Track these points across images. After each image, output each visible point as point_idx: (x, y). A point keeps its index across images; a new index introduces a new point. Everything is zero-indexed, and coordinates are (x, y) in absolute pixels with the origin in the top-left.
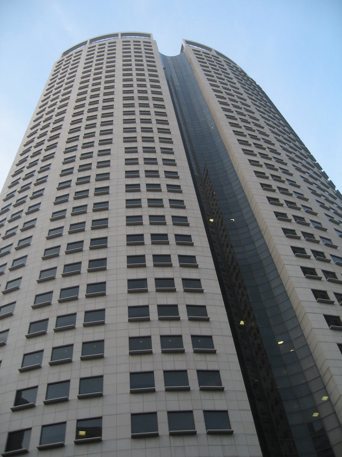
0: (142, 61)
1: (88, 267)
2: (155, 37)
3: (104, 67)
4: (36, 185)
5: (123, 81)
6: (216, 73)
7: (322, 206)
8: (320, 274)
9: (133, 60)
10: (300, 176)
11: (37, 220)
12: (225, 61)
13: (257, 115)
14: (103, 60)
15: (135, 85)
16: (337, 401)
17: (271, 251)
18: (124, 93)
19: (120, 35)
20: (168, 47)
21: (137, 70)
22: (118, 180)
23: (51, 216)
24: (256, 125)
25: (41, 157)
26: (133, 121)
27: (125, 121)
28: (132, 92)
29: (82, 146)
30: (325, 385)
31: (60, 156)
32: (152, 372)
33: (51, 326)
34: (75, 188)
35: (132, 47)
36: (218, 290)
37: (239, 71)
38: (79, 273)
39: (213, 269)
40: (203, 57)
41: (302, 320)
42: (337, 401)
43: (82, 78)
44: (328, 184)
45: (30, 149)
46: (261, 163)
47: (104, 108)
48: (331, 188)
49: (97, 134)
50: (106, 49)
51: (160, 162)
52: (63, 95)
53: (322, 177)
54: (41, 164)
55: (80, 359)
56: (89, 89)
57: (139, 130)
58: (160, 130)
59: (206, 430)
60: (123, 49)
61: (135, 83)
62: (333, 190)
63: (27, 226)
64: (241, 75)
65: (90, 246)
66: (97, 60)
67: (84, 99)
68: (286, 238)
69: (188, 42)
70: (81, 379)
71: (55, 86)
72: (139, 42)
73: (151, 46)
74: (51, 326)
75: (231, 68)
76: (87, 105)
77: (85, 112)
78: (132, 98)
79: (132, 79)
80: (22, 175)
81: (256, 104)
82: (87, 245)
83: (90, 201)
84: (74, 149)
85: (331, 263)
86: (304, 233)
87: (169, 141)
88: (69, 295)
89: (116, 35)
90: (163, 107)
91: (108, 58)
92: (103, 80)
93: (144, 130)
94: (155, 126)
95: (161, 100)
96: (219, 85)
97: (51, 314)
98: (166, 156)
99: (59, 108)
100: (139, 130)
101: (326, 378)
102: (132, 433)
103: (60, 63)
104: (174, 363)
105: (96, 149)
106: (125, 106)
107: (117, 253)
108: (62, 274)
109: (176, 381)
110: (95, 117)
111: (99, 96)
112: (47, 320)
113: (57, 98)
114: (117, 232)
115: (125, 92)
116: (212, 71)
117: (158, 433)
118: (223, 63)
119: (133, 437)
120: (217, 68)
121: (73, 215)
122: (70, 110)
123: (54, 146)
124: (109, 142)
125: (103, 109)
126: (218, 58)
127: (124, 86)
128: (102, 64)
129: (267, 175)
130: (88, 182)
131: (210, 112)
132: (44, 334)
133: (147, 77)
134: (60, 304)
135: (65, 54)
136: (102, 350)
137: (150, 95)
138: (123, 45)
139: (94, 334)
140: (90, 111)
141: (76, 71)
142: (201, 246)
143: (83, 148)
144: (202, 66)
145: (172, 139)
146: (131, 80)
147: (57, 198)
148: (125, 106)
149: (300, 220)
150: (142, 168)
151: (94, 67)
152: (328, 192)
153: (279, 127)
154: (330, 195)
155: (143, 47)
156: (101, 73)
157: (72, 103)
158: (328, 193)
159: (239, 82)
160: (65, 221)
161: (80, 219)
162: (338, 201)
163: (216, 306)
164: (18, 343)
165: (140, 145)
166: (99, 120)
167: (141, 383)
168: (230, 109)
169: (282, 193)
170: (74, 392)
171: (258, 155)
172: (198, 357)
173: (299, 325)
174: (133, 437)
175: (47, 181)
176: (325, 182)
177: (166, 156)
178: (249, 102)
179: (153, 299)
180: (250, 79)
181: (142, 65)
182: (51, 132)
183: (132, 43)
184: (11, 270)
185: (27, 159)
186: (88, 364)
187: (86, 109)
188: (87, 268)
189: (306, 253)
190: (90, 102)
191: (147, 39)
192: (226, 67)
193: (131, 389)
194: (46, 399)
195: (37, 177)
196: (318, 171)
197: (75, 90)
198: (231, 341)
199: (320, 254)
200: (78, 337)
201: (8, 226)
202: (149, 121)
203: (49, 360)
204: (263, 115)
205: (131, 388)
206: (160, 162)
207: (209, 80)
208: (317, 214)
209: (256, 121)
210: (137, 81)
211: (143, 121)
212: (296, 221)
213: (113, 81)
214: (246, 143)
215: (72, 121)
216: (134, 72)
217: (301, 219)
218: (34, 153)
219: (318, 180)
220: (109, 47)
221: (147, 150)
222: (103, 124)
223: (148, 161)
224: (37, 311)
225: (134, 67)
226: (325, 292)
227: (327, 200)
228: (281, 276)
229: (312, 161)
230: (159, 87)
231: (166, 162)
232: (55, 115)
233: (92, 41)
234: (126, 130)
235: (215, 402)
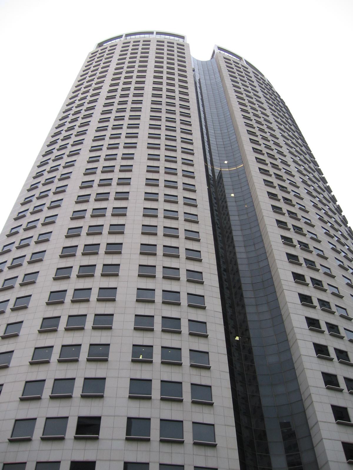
1: (105, 249)
2: (188, 40)
3: (136, 67)
4: (76, 136)
5: (155, 72)
6: (236, 66)
7: (321, 219)
8: (302, 261)
9: (165, 63)
10: (322, 227)
11: (46, 253)
12: (254, 72)
13: (274, 126)
14: (138, 49)
15: (164, 90)
16: (314, 426)
17: (273, 274)
18: (154, 78)
19: (155, 33)
20: (200, 52)
21: (168, 54)
22: (138, 188)
23: (81, 184)
24: (272, 135)
25: (74, 132)
26: (160, 103)
27: (154, 95)
28: (162, 72)
30: (305, 409)
31: (85, 154)
32: (149, 419)
33: (63, 324)
34: (96, 190)
35: (166, 48)
36: (219, 308)
37: (265, 84)
38: (97, 253)
39: (217, 287)
40: (233, 66)
41: (292, 345)
42: (314, 426)
44: (330, 198)
45: (69, 116)
46: (264, 152)
48: (322, 182)
49: (128, 110)
50: (140, 47)
51: (180, 173)
53: (311, 163)
54: (66, 159)
55: (86, 360)
57: (163, 137)
58: (182, 106)
59: (189, 331)
60: (157, 49)
61: (165, 65)
62: (328, 194)
63: (53, 204)
64: (267, 87)
65: (88, 357)
67: (121, 73)
68: (294, 283)
69: (220, 48)
70: (85, 379)
71: (97, 55)
72: (173, 43)
73: (184, 49)
74: (63, 324)
75: (256, 76)
77: (114, 112)
78: (161, 83)
79: (163, 61)
80: (52, 156)
81: (278, 121)
82: (102, 249)
83: (111, 204)
84: (107, 120)
85: (326, 292)
86: (299, 242)
88: (87, 272)
89: (152, 33)
90: (186, 88)
91: (141, 57)
92: (139, 55)
93: (168, 104)
95: (186, 88)
96: (242, 92)
97: (71, 285)
98: (186, 168)
99: (98, 78)
100: (163, 137)
101: (306, 404)
102: (126, 435)
103: (94, 54)
104: (171, 374)
105: (122, 141)
107: (130, 261)
108: (77, 275)
109: (171, 392)
111: (131, 84)
112: (60, 317)
113: (95, 75)
114: (132, 239)
115: (155, 77)
116: (238, 77)
117: (150, 438)
118: (251, 74)
119: (130, 397)
120: (243, 74)
121: (92, 216)
123: (90, 116)
124: (137, 126)
125: (136, 83)
127: (156, 67)
128: (138, 45)
129: (267, 162)
130: (113, 171)
131: (312, 448)
132: (62, 302)
133: (176, 82)
134: (72, 304)
135: (100, 45)
136: (111, 322)
137: (177, 77)
138: (157, 45)
139: (101, 337)
140: (123, 90)
141: (110, 62)
142: (209, 263)
143: (113, 129)
144: (229, 71)
146: (162, 67)
147: (87, 169)
149: (287, 201)
152: (323, 195)
153: (283, 119)
154: (330, 209)
155: (175, 49)
156: (137, 53)
157: (110, 76)
158: (317, 185)
159: (258, 81)
160: (84, 222)
161: (98, 221)
162: (349, 242)
163: (215, 323)
164: (20, 370)
165: (163, 153)
166: (130, 99)
167: (139, 390)
169: (290, 217)
170: (84, 354)
171: (273, 176)
172: (194, 371)
173: (290, 349)
174: (130, 397)
175: (61, 205)
176: (313, 167)
177: (186, 168)
178: (268, 112)
179: (158, 340)
180: (275, 93)
181: (173, 59)
182: (88, 103)
183: (166, 44)
184: (30, 263)
185: (65, 123)
186: (98, 333)
188: (87, 357)
189: (339, 386)
190: (119, 102)
191: (181, 41)
192: (253, 79)
193: (130, 395)
194: (60, 358)
195: (62, 172)
196: (314, 167)
197: (106, 87)
198: (225, 359)
199: (325, 304)
200: (87, 338)
201: (8, 274)
202: (173, 105)
203: (50, 394)
204: (271, 106)
205: (129, 394)
206: (180, 173)
208: (315, 226)
209: (263, 110)
210: (167, 74)
211: (168, 104)
212: (294, 230)
214: (253, 134)
215: (105, 104)
216: (165, 52)
217: (298, 229)
218: (68, 128)
219: (316, 184)
220: (143, 45)
222: (134, 102)
223: (169, 148)
224: (51, 308)
225: (165, 70)
226: (318, 321)
227: (326, 213)
228: (279, 299)
229: (319, 175)
230: (186, 77)
232: (85, 110)
233: (127, 35)
234: (153, 103)
235: (204, 416)
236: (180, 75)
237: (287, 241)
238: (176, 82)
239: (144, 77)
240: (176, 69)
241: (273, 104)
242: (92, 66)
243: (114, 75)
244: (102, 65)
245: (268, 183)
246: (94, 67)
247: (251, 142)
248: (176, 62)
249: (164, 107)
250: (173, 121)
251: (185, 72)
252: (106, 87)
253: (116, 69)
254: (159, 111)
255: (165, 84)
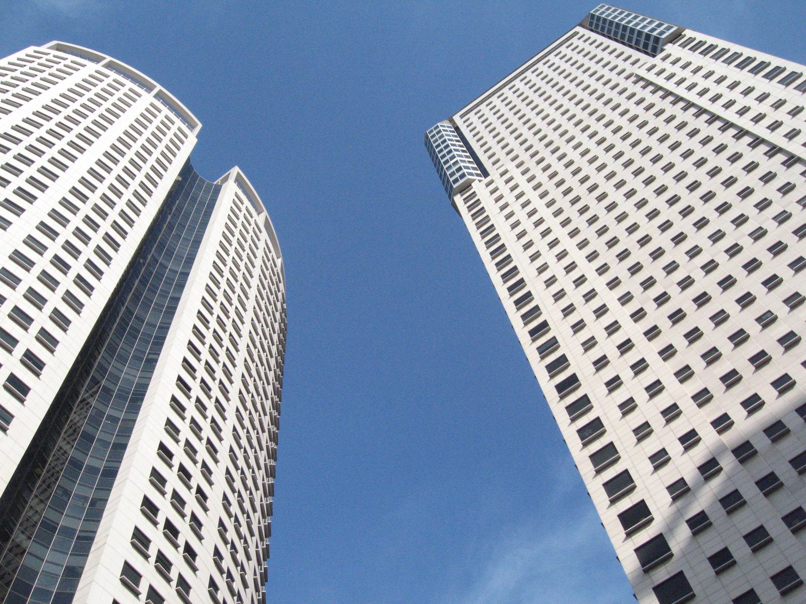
0: (169, 128)
15: (121, 165)
28: (129, 147)
29: (3, 164)
43: (70, 90)
47: (63, 152)
52: (58, 70)
56: (88, 95)
58: (123, 214)
61: (142, 140)
66: (109, 85)
73: (182, 143)
76: (22, 145)
78: (122, 154)
87: (98, 273)
90: (137, 212)
92: (113, 99)
94: (105, 227)
95: (150, 193)
106: (100, 163)
110: (29, 162)
122: (46, 98)
126: (260, 232)
128: (117, 90)
145: (95, 290)
146: (145, 127)
148: (107, 155)
150: (43, 263)
151: (91, 95)
166: (30, 171)
168: (223, 270)
181: (169, 128)
187: (38, 133)
207: (230, 218)
213: (104, 129)
215: (37, 112)
221: (69, 247)
231: (69, 298)
234: (75, 191)
236: (158, 161)
237: (140, 541)
238: (146, 168)
239: (97, 135)
240: (159, 150)
241: (271, 260)
242: (20, 69)
243: (69, 90)
244: (53, 71)
245: (172, 429)
246: (47, 60)
247: (214, 266)
248: (166, 140)
249: (76, 221)
250: (85, 239)
251: (174, 155)
252: (46, 98)
253: (70, 90)
254: (52, 234)
255: (114, 174)
